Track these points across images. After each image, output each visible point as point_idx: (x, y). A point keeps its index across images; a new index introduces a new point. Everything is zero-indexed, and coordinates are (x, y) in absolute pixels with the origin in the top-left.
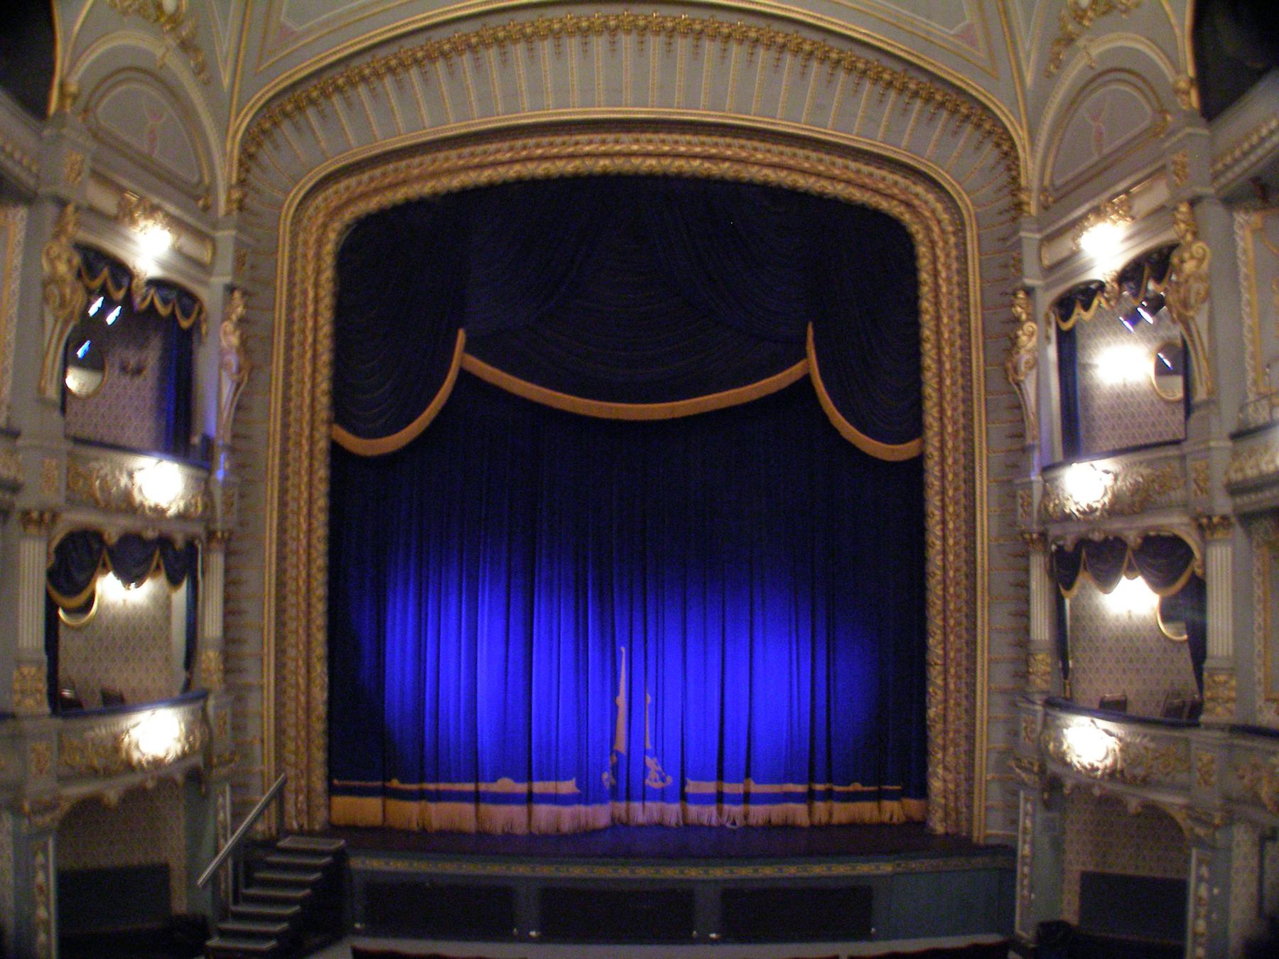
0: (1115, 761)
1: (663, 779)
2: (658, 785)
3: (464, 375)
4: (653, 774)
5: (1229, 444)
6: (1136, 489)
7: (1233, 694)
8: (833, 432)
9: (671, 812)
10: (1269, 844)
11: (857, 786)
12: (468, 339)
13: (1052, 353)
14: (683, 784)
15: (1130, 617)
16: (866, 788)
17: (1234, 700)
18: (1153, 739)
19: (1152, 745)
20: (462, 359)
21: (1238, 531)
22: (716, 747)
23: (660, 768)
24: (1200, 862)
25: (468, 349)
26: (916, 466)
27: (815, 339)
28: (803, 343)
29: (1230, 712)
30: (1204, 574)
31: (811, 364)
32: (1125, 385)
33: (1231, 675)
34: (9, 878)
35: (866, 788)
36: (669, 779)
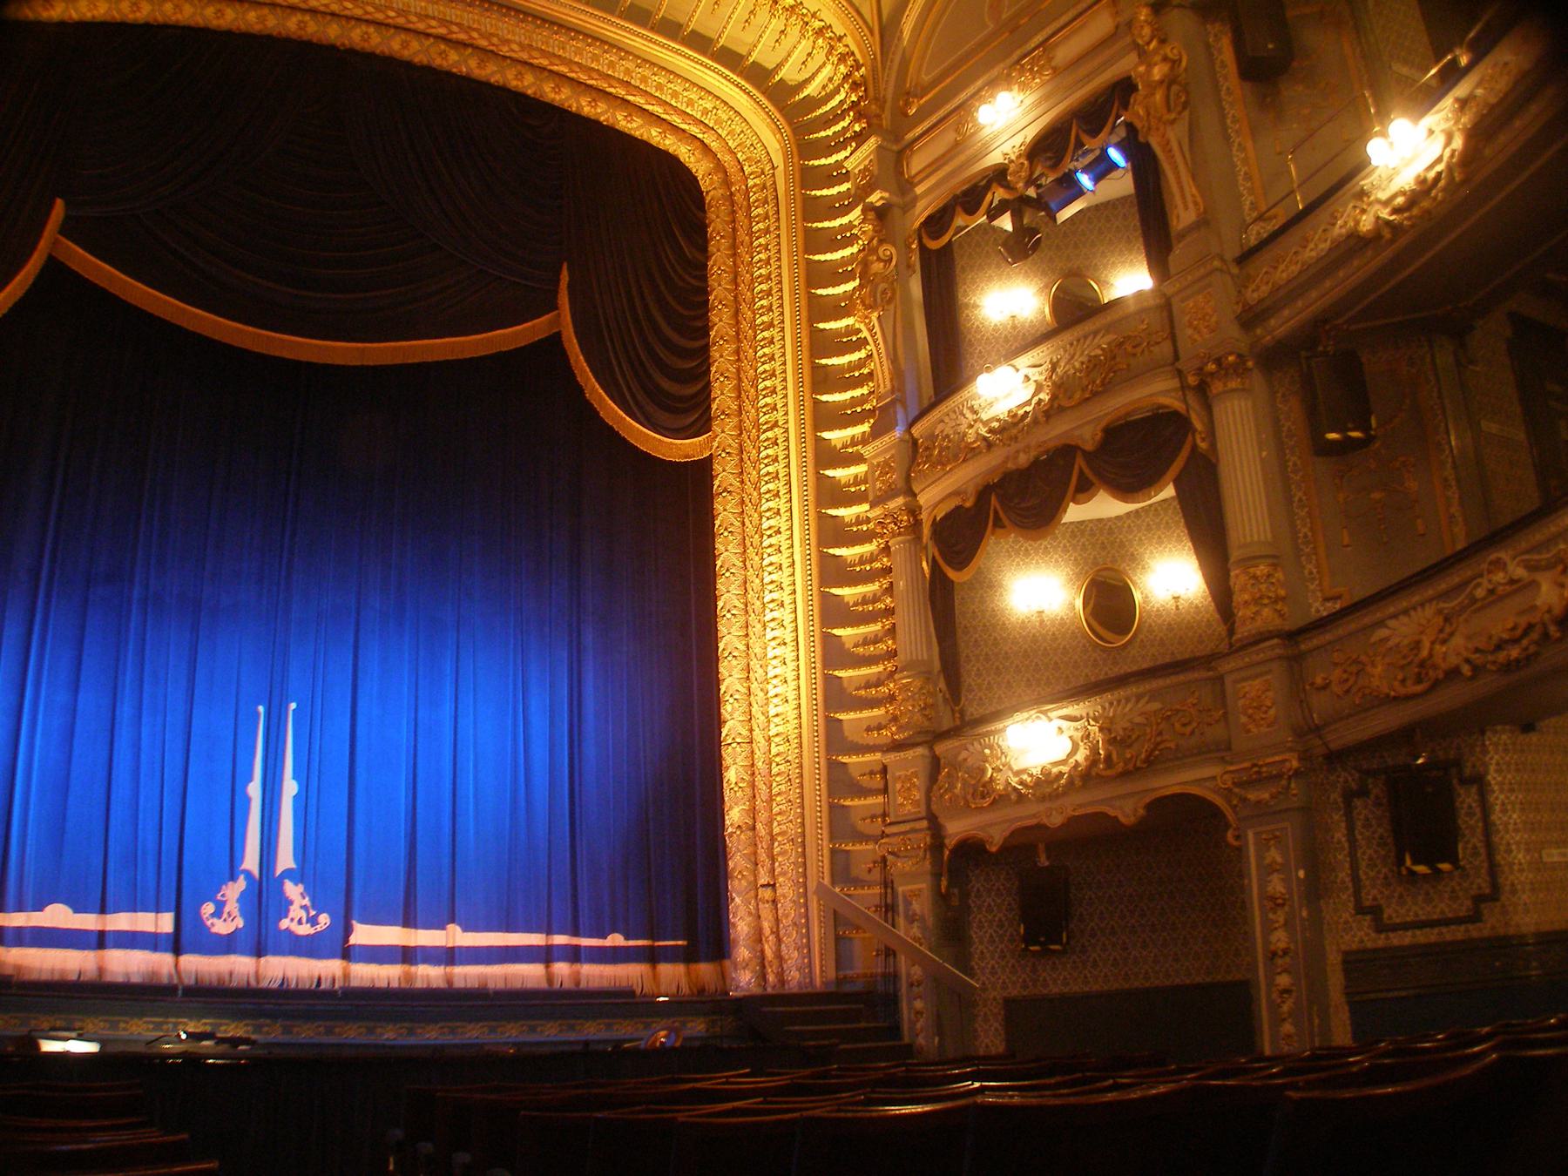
0: (1094, 750)
1: (313, 921)
2: (305, 930)
3: (53, 266)
4: (296, 912)
5: (1235, 270)
6: (1093, 365)
7: (1282, 592)
8: (589, 412)
9: (329, 969)
10: (1358, 802)
11: (616, 940)
12: (67, 218)
13: (916, 288)
14: (348, 931)
15: (1042, 622)
16: (631, 943)
17: (1283, 599)
18: (1153, 696)
19: (1156, 706)
20: (56, 243)
21: (1257, 380)
22: (402, 867)
23: (306, 901)
24: (1263, 846)
25: (67, 230)
26: (703, 469)
27: (569, 286)
28: (555, 293)
29: (1281, 616)
30: (1213, 446)
31: (563, 320)
32: (1014, 327)
33: (1274, 566)
34: (56, 13)
35: (631, 943)
36: (324, 919)
